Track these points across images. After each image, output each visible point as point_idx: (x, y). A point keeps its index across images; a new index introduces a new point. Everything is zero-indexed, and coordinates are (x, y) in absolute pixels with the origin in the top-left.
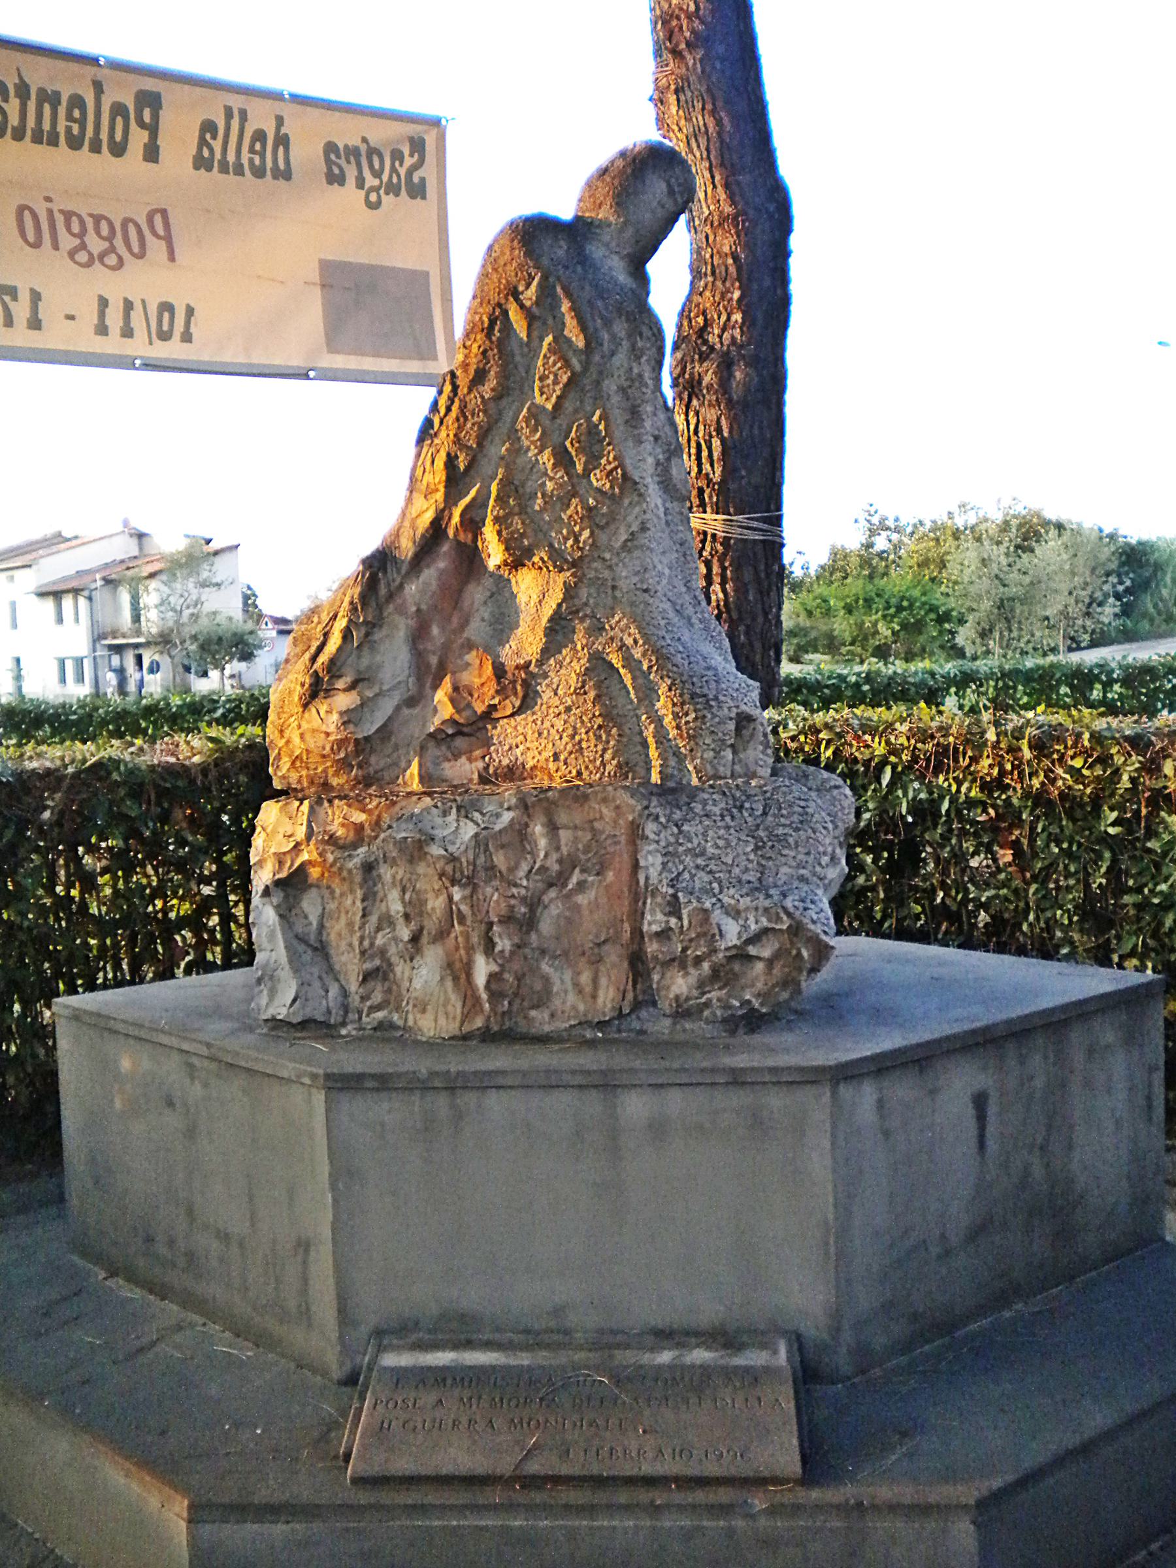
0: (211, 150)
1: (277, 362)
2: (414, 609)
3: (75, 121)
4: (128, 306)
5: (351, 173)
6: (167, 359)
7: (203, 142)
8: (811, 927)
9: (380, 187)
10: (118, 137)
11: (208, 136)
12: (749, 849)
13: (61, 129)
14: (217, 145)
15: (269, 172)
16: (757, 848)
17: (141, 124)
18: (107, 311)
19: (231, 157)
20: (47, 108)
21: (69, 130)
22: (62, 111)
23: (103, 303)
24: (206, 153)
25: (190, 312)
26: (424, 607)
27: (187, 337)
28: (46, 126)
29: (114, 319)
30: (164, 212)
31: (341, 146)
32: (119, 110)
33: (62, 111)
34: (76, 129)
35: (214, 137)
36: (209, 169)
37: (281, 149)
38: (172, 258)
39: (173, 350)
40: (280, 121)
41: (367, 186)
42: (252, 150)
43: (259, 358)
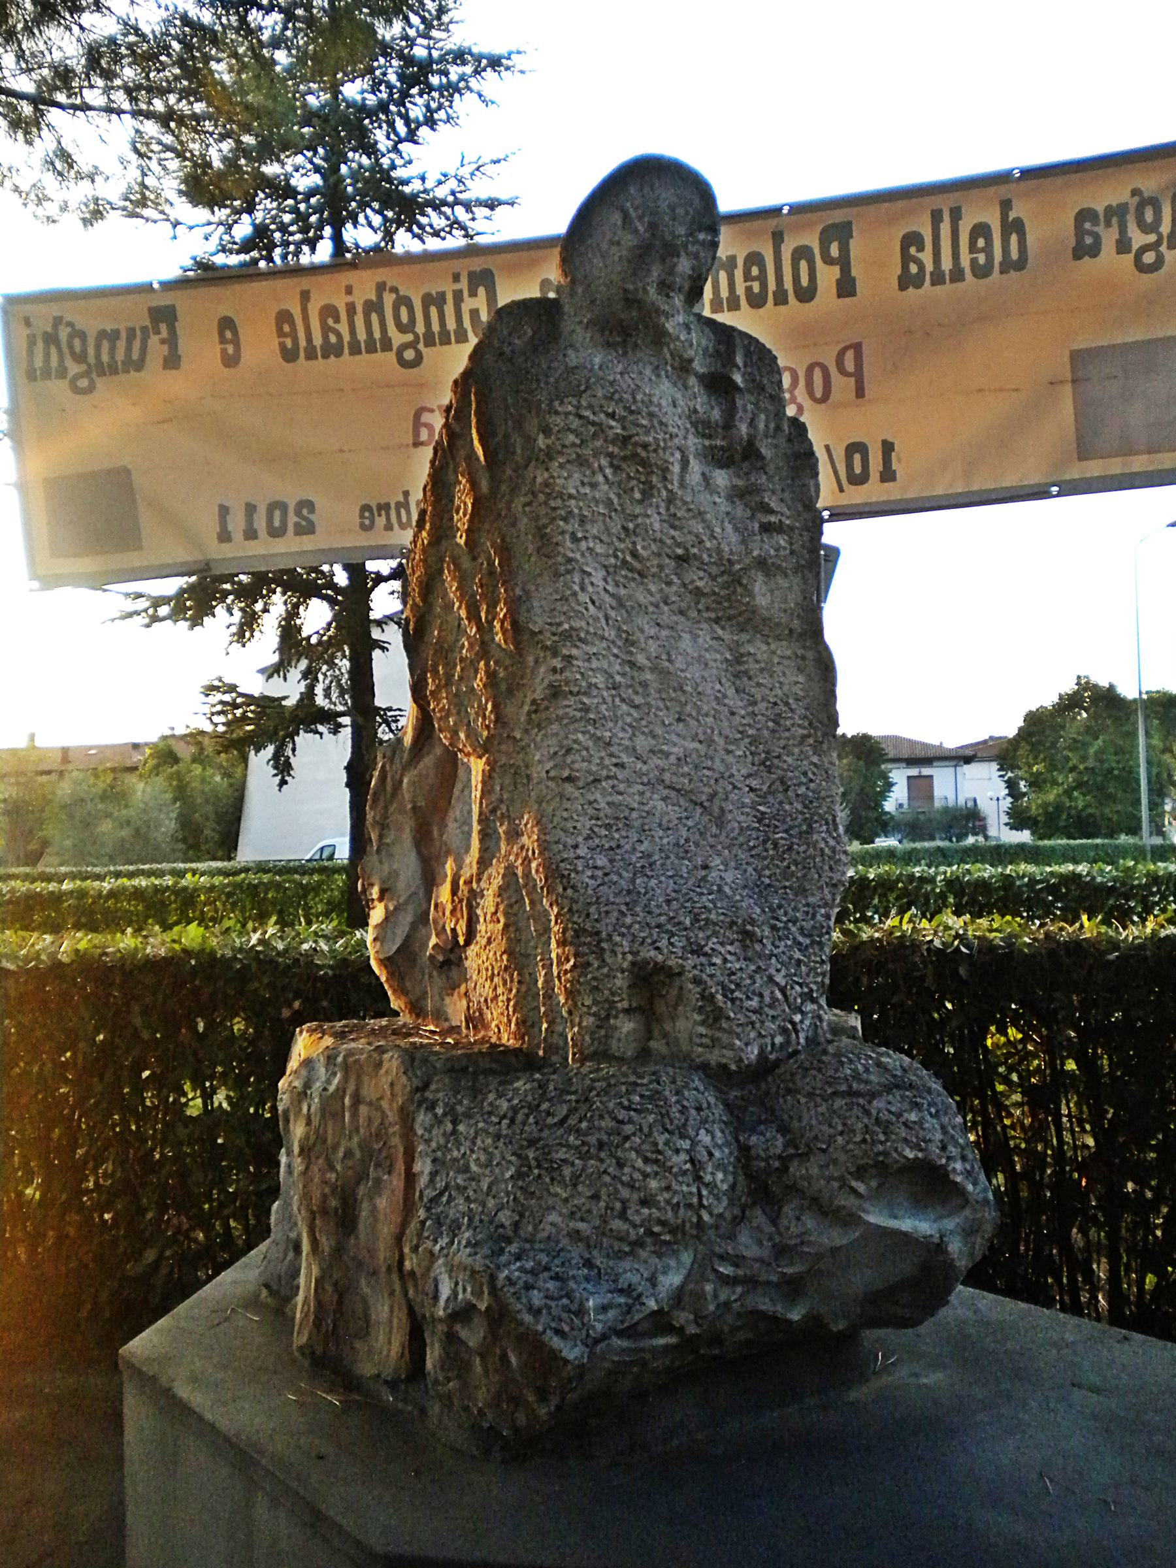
0: (339, 335)
1: (1007, 484)
2: (409, 806)
3: (286, 335)
4: (251, 509)
5: (1109, 237)
6: (917, 499)
7: (906, 258)
8: (528, 1318)
9: (1158, 243)
10: (805, 282)
11: (330, 322)
12: (508, 1175)
13: (740, 290)
14: (926, 257)
15: (302, 354)
16: (519, 1175)
17: (828, 260)
18: (229, 518)
19: (362, 336)
20: (433, 311)
21: (749, 290)
22: (739, 274)
23: (224, 511)
24: (333, 339)
25: (888, 448)
26: (421, 803)
27: (888, 475)
28: (436, 327)
29: (237, 524)
30: (857, 348)
31: (1100, 209)
32: (802, 253)
33: (739, 274)
34: (289, 343)
35: (337, 321)
36: (339, 354)
37: (1014, 238)
38: (860, 392)
39: (873, 491)
40: (1006, 205)
41: (1135, 246)
42: (973, 248)
43: (980, 483)
